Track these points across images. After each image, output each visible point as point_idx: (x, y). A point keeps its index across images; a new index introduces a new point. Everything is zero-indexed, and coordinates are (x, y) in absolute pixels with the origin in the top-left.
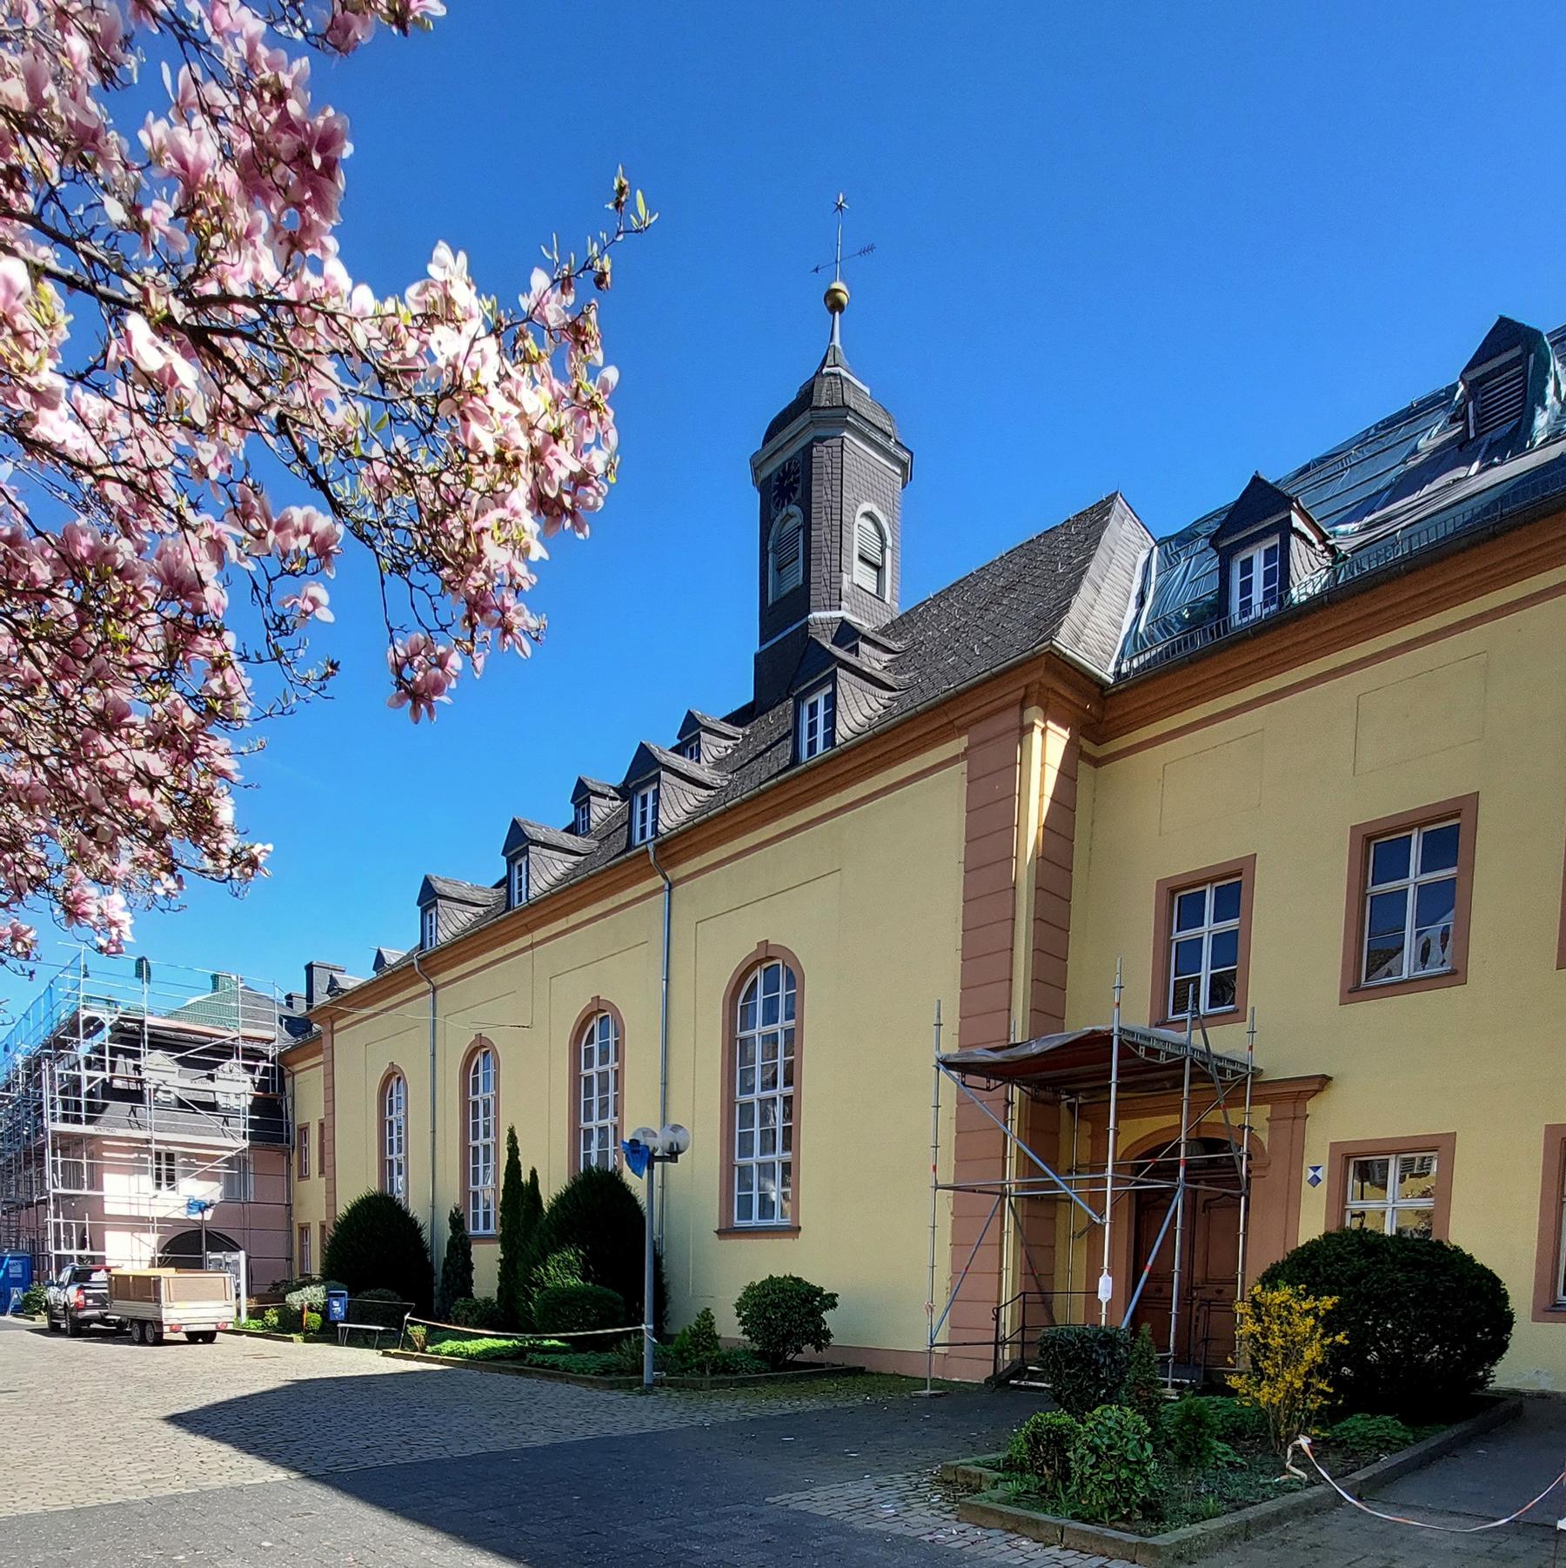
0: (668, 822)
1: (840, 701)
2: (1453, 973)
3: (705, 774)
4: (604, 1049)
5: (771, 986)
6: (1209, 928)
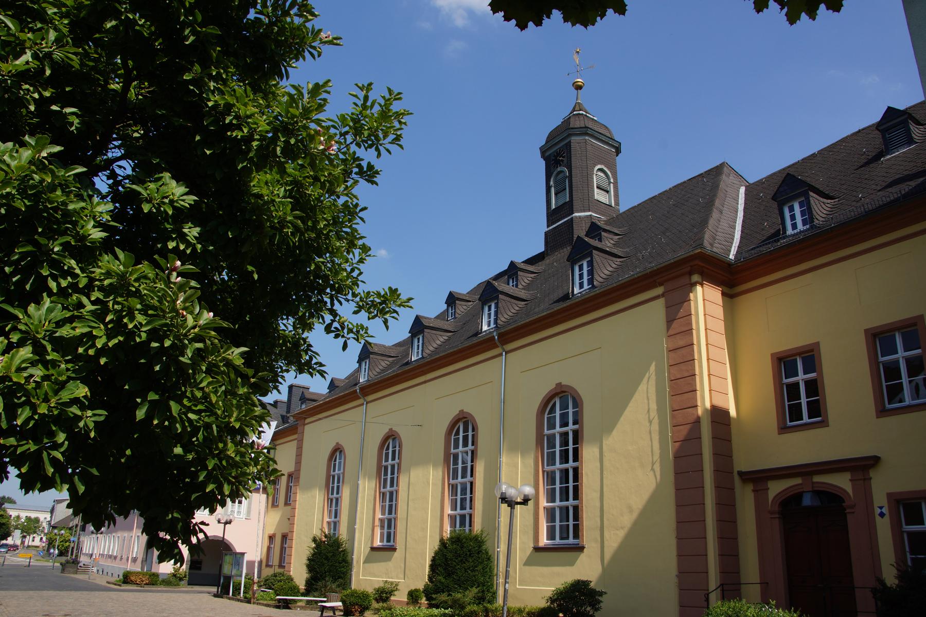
0: (503, 319)
1: (595, 264)
3: (522, 294)
4: (465, 438)
5: (564, 406)
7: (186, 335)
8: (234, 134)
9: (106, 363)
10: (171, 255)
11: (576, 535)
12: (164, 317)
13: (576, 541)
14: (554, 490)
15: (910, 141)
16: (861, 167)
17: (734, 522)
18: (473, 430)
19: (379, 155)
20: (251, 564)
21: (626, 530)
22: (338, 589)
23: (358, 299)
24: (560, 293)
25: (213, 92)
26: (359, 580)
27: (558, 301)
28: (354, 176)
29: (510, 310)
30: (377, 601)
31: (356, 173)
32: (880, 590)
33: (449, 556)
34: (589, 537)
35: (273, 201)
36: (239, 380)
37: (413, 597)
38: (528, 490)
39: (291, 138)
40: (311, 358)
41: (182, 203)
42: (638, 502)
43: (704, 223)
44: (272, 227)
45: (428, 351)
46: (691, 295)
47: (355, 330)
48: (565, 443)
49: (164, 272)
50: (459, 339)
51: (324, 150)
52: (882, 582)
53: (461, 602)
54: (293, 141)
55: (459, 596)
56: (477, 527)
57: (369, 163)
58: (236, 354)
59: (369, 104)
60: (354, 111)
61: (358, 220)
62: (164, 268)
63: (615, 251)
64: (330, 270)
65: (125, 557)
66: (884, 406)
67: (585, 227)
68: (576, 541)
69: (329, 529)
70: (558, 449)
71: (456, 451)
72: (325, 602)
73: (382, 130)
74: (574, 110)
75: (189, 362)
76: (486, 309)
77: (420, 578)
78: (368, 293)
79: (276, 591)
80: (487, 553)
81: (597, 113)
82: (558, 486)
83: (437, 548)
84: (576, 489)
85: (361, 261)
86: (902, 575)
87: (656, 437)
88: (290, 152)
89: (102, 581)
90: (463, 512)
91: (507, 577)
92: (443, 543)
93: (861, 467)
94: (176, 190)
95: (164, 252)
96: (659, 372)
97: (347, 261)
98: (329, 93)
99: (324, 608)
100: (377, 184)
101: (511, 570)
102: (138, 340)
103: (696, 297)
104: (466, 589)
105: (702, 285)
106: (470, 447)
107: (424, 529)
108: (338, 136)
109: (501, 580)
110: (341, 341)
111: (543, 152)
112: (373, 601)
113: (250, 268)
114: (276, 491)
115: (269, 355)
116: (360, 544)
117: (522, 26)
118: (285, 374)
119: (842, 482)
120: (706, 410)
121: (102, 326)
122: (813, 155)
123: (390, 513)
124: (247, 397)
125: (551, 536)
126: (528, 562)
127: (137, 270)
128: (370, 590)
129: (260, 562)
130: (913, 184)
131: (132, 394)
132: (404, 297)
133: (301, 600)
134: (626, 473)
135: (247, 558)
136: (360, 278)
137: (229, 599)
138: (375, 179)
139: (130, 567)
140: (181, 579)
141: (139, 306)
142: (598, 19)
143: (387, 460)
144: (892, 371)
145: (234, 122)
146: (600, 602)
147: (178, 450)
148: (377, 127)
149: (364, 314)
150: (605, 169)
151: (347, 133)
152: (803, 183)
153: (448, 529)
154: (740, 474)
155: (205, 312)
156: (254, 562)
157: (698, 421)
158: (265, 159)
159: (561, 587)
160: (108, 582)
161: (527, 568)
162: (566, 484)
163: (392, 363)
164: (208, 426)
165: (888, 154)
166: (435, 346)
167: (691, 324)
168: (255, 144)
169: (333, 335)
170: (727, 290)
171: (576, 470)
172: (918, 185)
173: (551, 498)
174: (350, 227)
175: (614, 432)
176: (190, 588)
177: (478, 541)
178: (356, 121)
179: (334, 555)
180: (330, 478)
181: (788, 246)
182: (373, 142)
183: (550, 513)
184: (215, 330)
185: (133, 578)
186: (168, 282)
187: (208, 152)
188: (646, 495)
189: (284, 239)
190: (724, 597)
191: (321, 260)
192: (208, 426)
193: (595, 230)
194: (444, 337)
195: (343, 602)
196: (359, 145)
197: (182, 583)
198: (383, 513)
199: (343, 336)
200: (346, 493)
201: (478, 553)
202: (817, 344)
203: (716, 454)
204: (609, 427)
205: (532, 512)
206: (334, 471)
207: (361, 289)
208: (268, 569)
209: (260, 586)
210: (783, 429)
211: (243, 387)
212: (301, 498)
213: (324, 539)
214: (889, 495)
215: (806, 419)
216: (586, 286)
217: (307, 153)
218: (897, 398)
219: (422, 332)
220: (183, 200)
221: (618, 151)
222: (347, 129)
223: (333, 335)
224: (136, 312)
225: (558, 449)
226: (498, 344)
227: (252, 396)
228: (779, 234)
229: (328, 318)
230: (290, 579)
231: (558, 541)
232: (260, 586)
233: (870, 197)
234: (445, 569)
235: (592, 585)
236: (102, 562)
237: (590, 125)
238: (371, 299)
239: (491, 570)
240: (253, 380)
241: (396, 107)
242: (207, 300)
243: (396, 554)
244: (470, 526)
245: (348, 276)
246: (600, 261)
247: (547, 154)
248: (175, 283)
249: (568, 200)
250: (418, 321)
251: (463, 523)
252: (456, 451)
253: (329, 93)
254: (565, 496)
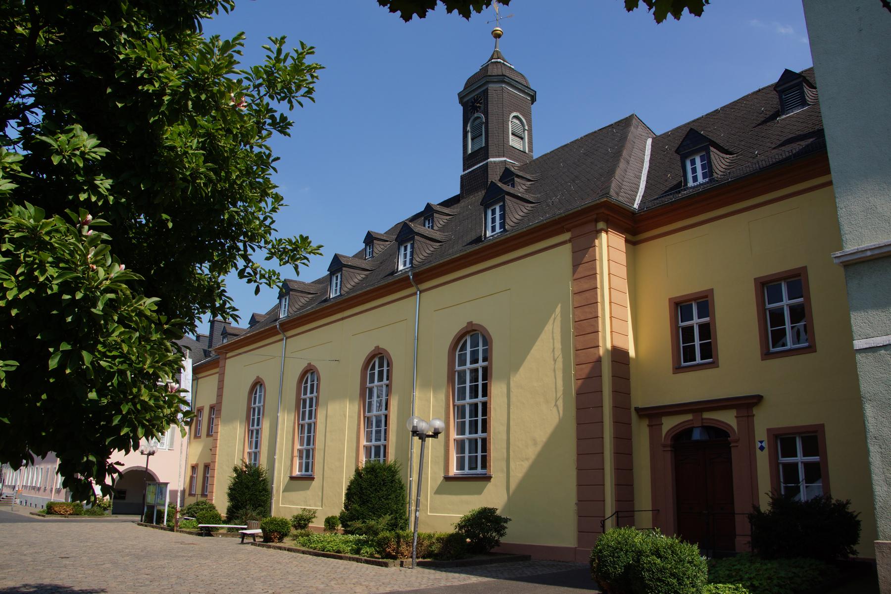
0: (418, 259)
1: (507, 209)
2: (809, 347)
3: (437, 235)
4: (381, 373)
5: (475, 344)
6: (696, 321)
7: (97, 288)
8: (146, 88)
9: (17, 314)
10: (82, 210)
11: (484, 466)
12: (76, 270)
13: (484, 471)
14: (464, 423)
15: (804, 103)
16: (759, 125)
17: (630, 454)
18: (388, 366)
19: (292, 107)
20: (174, 493)
21: (531, 461)
22: (258, 517)
23: (270, 246)
24: (473, 236)
25: (124, 45)
26: (278, 508)
27: (471, 243)
28: (267, 127)
29: (425, 251)
30: (296, 527)
31: (269, 124)
32: (756, 517)
33: (364, 485)
34: (496, 467)
35: (187, 152)
36: (153, 326)
37: (330, 524)
38: (439, 424)
39: (202, 94)
40: (225, 303)
41: (93, 155)
42: (542, 435)
43: (611, 173)
44: (184, 179)
45: (346, 289)
46: (597, 241)
47: (267, 276)
48: (475, 379)
49: (75, 227)
50: (376, 277)
51: (234, 107)
52: (757, 508)
53: (374, 529)
54: (203, 97)
55: (373, 523)
56: (391, 458)
57: (282, 115)
58: (149, 303)
59: (282, 57)
60: (268, 64)
61: (271, 171)
62: (76, 221)
63: (527, 197)
64: (243, 218)
65: (48, 488)
66: (768, 349)
67: (499, 172)
68: (484, 471)
69: (250, 459)
70: (468, 384)
71: (371, 385)
72: (245, 529)
73: (295, 83)
74: (492, 58)
75: (101, 313)
76: (402, 249)
77: (337, 508)
78: (280, 240)
79: (198, 520)
80: (400, 482)
81: (514, 62)
82: (467, 419)
83: (352, 478)
84: (485, 422)
85: (274, 210)
86: (776, 502)
87: (560, 375)
88: (201, 108)
89: (25, 512)
90: (378, 443)
91: (417, 505)
92: (358, 473)
93: (746, 405)
94: (88, 142)
95: (76, 205)
96: (564, 315)
97: (260, 209)
98: (242, 45)
99: (244, 536)
100: (289, 135)
101: (422, 498)
102: (49, 292)
103: (601, 244)
104: (380, 516)
105: (607, 232)
106: (385, 381)
107: (341, 460)
108: (252, 88)
109: (413, 508)
110: (253, 285)
111: (462, 97)
112: (292, 528)
113: (164, 216)
114: (199, 423)
115: (185, 298)
116: (280, 473)
117: (407, 17)
118: (202, 315)
119: (729, 418)
120: (607, 350)
121: (13, 278)
122: (716, 111)
123: (308, 444)
124: (160, 343)
125: (461, 466)
126: (439, 491)
127: (47, 224)
128: (289, 517)
129: (183, 492)
130: (804, 143)
131: (45, 344)
132: (314, 245)
133: (222, 528)
134: (532, 409)
135: (169, 488)
136: (272, 226)
137: (153, 527)
138: (287, 130)
139: (54, 498)
140: (105, 509)
141: (50, 259)
142: (484, 6)
143: (305, 394)
144: (777, 317)
145: (146, 76)
146: (505, 528)
147: (93, 395)
148: (290, 80)
149: (275, 260)
151: (260, 85)
152: (704, 138)
153: (363, 459)
154: (637, 409)
155: (117, 265)
156: (177, 491)
157: (599, 360)
158: (176, 113)
159: (469, 514)
160: (31, 513)
161: (438, 496)
162: (475, 418)
163: (312, 300)
164: (122, 373)
165: (783, 114)
166: (353, 284)
167: (595, 269)
168: (166, 98)
169: (246, 280)
170: (630, 237)
171: (485, 405)
172: (807, 146)
173: (461, 431)
174: (263, 178)
175: (521, 370)
176: (114, 517)
177: (392, 471)
178: (269, 73)
179: (254, 485)
180: (250, 410)
181: (689, 197)
182: (287, 94)
183: (460, 445)
184: (127, 282)
185: (56, 509)
186: (79, 235)
187: (120, 105)
188: (549, 429)
189: (197, 189)
190: (618, 525)
191: (235, 209)
192: (122, 373)
193: (508, 175)
194: (363, 275)
195: (263, 529)
196: (272, 97)
197: (107, 512)
198: (302, 444)
199: (255, 281)
200: (266, 425)
201: (392, 482)
202: (712, 290)
203: (615, 392)
204: (515, 366)
205: (443, 443)
206: (255, 403)
207: (273, 237)
208: (191, 498)
209: (183, 515)
210: (678, 369)
211: (156, 333)
212: (222, 430)
213: (245, 469)
214: (769, 430)
215: (698, 360)
216: (498, 230)
217: (218, 108)
218: (781, 343)
219: (340, 270)
220: (95, 153)
221: (533, 99)
222: (261, 81)
223: (246, 280)
224: (48, 265)
225: (468, 384)
226: (413, 283)
227: (166, 341)
228: (680, 185)
229: (241, 263)
230: (213, 508)
231: (467, 471)
232: (183, 515)
233: (765, 154)
234: (360, 498)
235: (498, 513)
236: (25, 493)
237: (507, 73)
238: (283, 246)
239: (404, 498)
240: (166, 327)
241: (308, 61)
242: (120, 252)
243: (314, 483)
244: (385, 456)
245: (262, 223)
246: (512, 206)
247: (465, 100)
248: (86, 237)
250: (336, 259)
251: (377, 454)
252: (371, 385)
253: (242, 45)
254: (474, 428)
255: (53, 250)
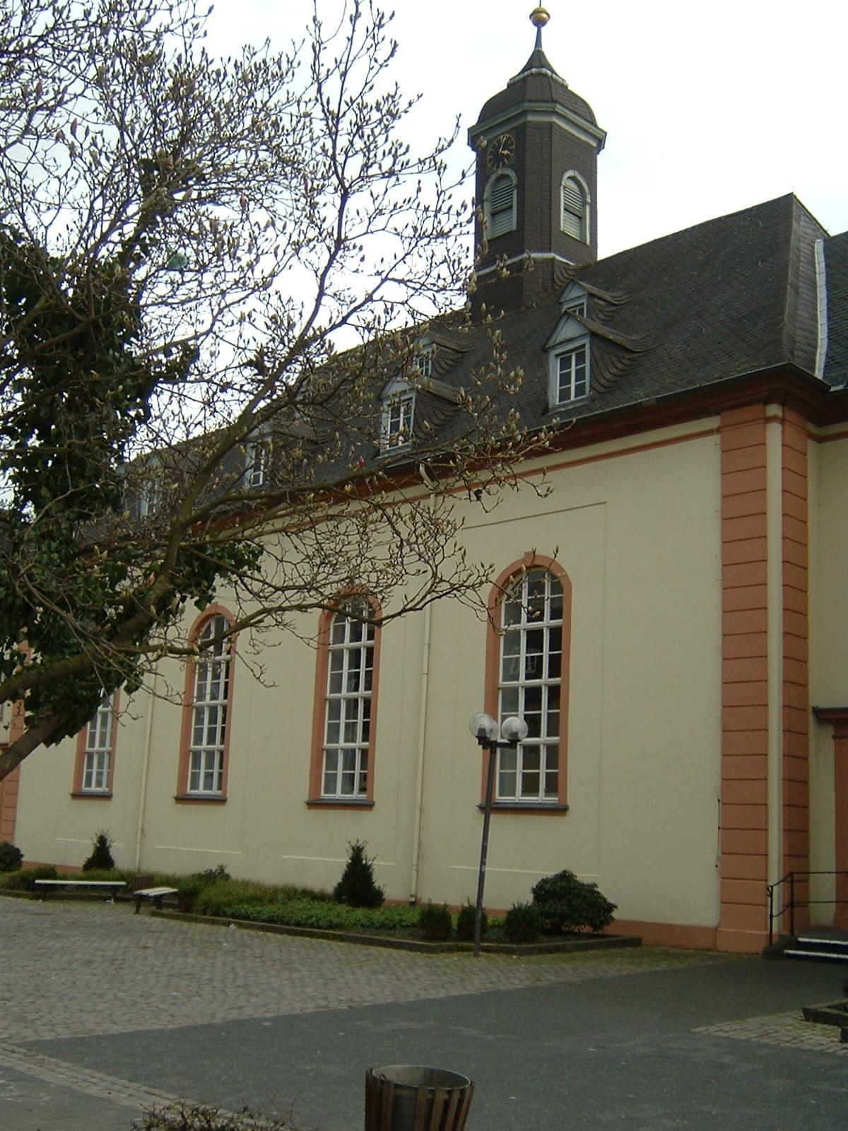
17: (805, 782)
68: (553, 800)
150: (579, 178)
154: (818, 712)
249: (514, 228)
255: (245, 392)
